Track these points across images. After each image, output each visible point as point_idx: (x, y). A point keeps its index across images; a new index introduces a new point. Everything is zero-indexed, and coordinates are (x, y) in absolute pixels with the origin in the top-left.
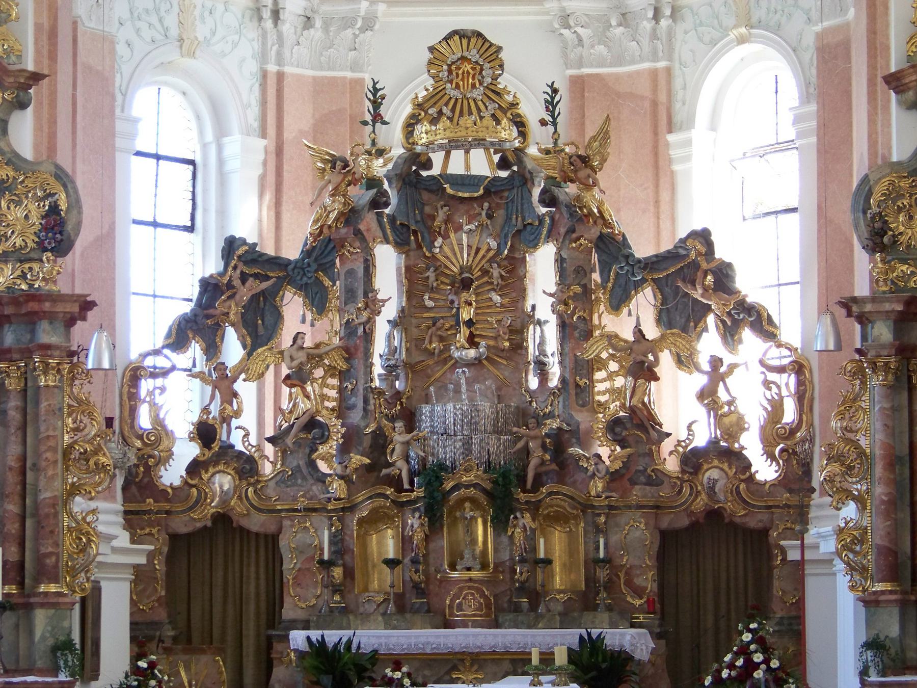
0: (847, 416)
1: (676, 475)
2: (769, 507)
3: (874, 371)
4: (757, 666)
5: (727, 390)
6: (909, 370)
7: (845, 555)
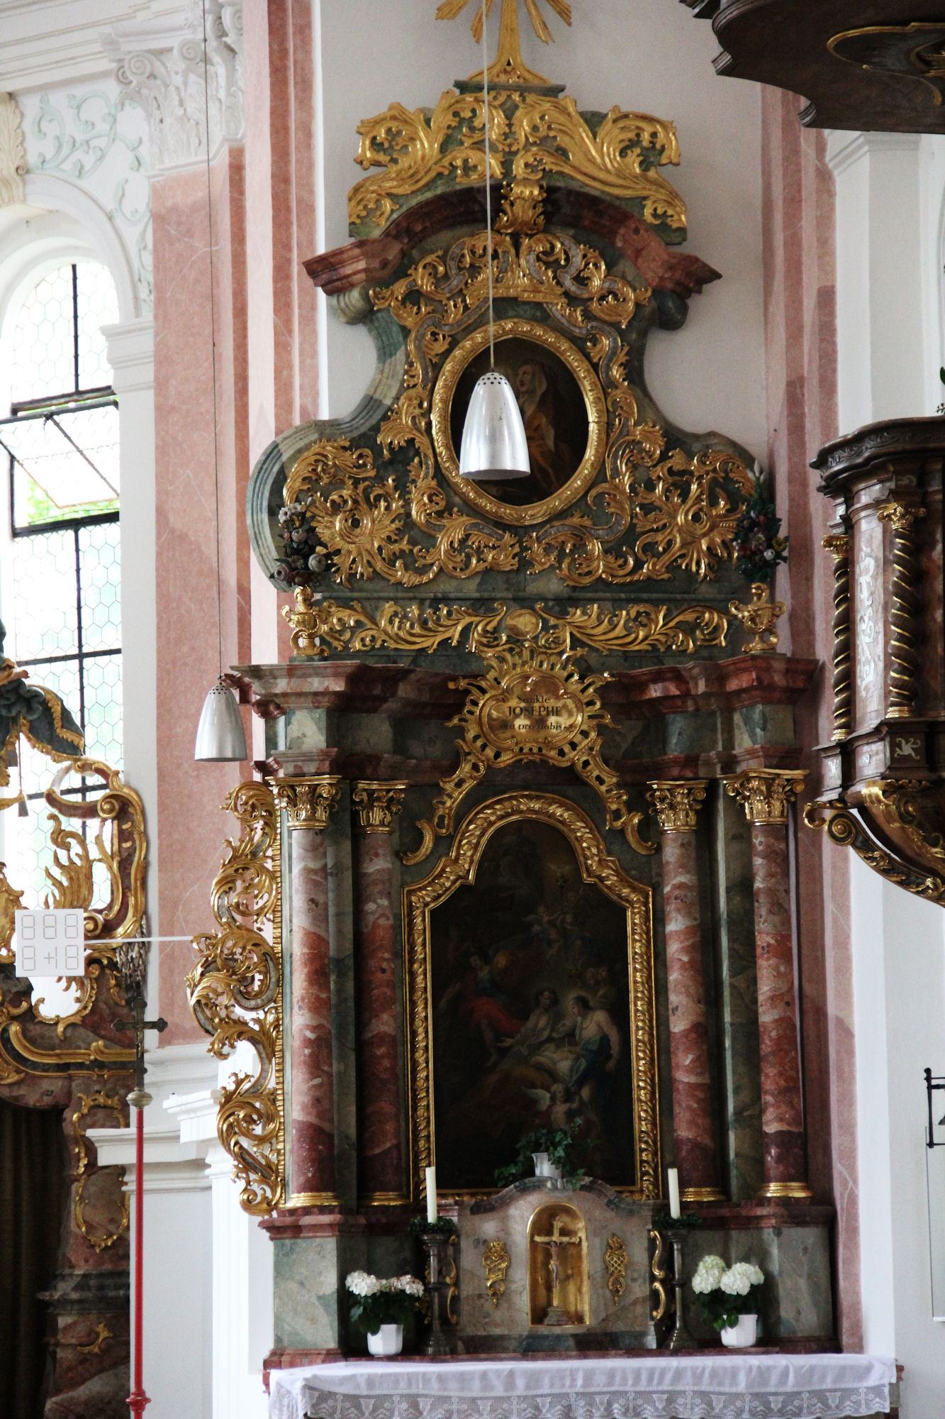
2: (66, 1067)
6: (353, 802)
7: (237, 1143)
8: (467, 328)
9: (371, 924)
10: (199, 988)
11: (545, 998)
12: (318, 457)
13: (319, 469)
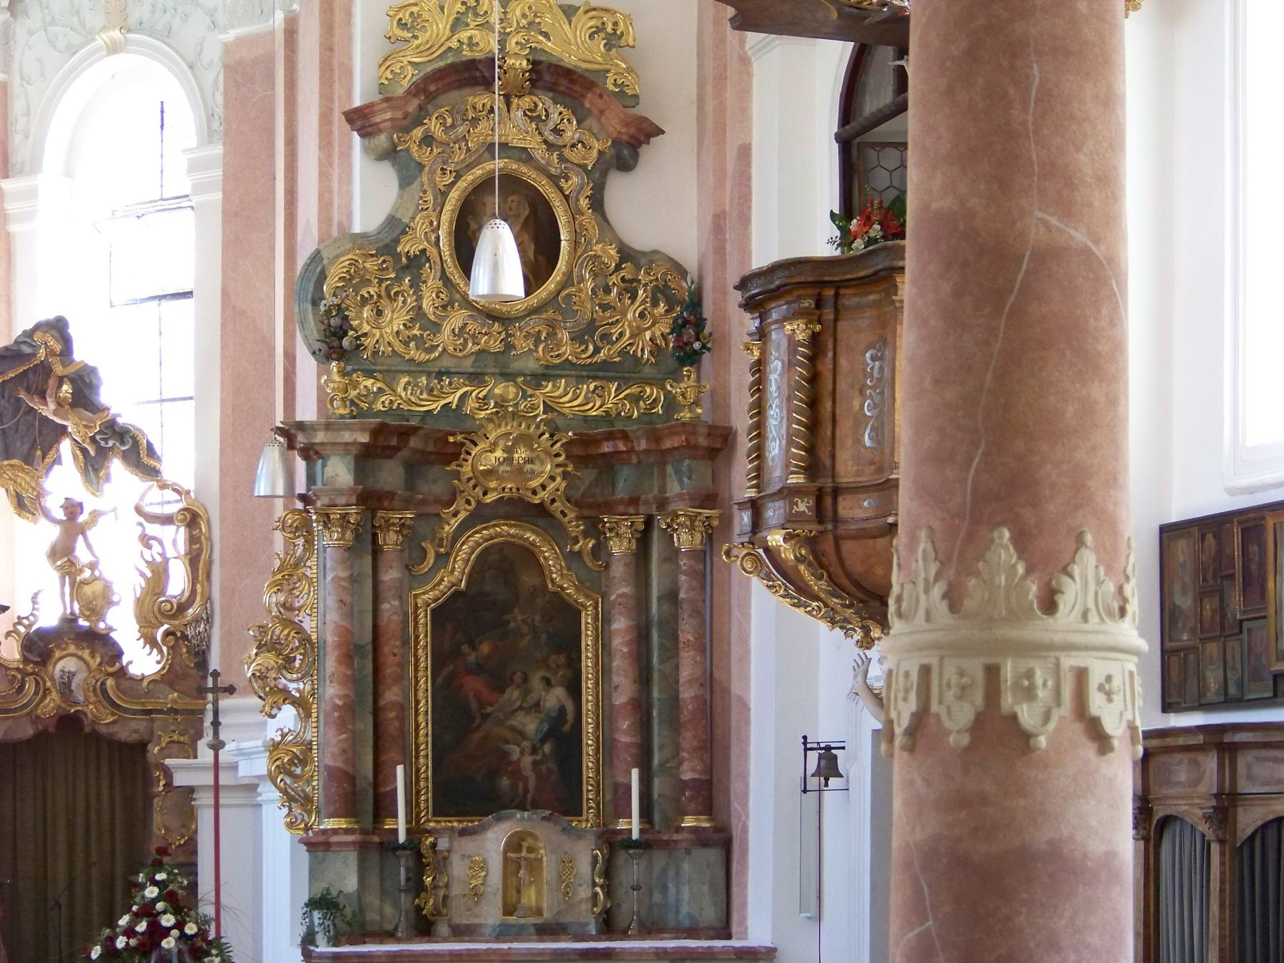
0: (286, 588)
1: (15, 665)
2: (149, 712)
3: (326, 526)
4: (166, 932)
5: (89, 546)
6: (374, 526)
7: (282, 780)
8: (468, 165)
9: (385, 620)
10: (254, 665)
11: (518, 678)
12: (352, 261)
13: (352, 271)
